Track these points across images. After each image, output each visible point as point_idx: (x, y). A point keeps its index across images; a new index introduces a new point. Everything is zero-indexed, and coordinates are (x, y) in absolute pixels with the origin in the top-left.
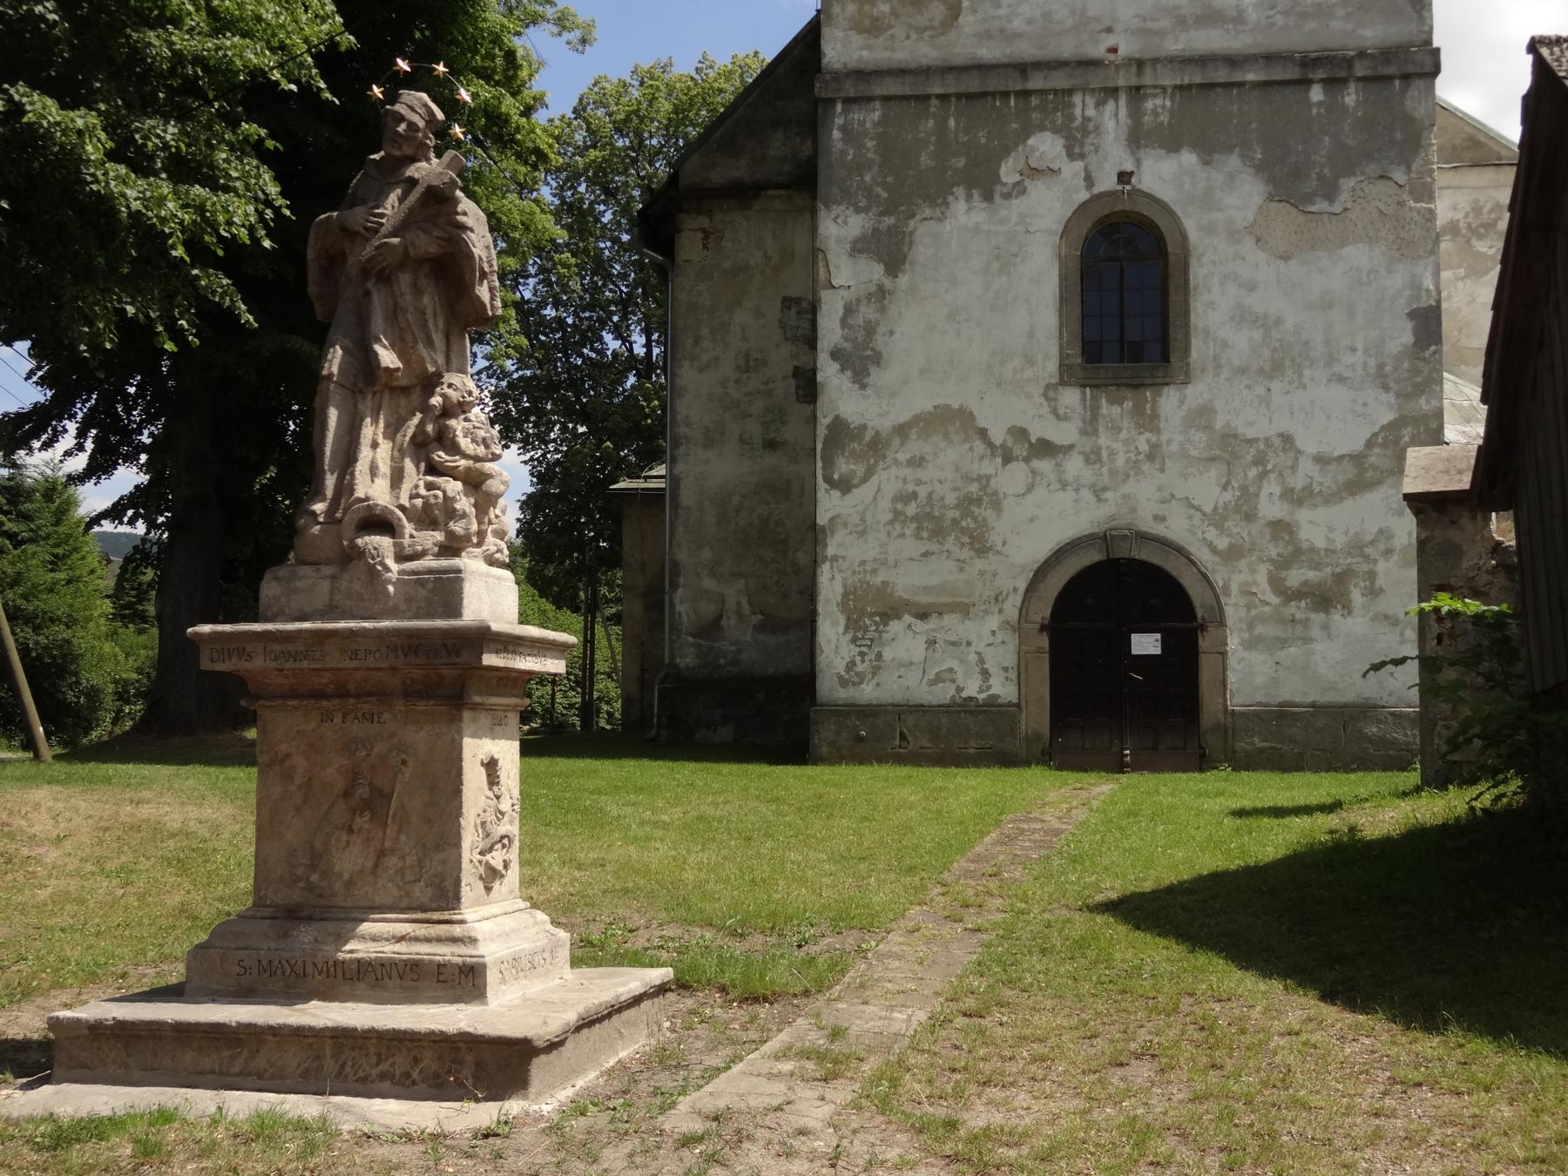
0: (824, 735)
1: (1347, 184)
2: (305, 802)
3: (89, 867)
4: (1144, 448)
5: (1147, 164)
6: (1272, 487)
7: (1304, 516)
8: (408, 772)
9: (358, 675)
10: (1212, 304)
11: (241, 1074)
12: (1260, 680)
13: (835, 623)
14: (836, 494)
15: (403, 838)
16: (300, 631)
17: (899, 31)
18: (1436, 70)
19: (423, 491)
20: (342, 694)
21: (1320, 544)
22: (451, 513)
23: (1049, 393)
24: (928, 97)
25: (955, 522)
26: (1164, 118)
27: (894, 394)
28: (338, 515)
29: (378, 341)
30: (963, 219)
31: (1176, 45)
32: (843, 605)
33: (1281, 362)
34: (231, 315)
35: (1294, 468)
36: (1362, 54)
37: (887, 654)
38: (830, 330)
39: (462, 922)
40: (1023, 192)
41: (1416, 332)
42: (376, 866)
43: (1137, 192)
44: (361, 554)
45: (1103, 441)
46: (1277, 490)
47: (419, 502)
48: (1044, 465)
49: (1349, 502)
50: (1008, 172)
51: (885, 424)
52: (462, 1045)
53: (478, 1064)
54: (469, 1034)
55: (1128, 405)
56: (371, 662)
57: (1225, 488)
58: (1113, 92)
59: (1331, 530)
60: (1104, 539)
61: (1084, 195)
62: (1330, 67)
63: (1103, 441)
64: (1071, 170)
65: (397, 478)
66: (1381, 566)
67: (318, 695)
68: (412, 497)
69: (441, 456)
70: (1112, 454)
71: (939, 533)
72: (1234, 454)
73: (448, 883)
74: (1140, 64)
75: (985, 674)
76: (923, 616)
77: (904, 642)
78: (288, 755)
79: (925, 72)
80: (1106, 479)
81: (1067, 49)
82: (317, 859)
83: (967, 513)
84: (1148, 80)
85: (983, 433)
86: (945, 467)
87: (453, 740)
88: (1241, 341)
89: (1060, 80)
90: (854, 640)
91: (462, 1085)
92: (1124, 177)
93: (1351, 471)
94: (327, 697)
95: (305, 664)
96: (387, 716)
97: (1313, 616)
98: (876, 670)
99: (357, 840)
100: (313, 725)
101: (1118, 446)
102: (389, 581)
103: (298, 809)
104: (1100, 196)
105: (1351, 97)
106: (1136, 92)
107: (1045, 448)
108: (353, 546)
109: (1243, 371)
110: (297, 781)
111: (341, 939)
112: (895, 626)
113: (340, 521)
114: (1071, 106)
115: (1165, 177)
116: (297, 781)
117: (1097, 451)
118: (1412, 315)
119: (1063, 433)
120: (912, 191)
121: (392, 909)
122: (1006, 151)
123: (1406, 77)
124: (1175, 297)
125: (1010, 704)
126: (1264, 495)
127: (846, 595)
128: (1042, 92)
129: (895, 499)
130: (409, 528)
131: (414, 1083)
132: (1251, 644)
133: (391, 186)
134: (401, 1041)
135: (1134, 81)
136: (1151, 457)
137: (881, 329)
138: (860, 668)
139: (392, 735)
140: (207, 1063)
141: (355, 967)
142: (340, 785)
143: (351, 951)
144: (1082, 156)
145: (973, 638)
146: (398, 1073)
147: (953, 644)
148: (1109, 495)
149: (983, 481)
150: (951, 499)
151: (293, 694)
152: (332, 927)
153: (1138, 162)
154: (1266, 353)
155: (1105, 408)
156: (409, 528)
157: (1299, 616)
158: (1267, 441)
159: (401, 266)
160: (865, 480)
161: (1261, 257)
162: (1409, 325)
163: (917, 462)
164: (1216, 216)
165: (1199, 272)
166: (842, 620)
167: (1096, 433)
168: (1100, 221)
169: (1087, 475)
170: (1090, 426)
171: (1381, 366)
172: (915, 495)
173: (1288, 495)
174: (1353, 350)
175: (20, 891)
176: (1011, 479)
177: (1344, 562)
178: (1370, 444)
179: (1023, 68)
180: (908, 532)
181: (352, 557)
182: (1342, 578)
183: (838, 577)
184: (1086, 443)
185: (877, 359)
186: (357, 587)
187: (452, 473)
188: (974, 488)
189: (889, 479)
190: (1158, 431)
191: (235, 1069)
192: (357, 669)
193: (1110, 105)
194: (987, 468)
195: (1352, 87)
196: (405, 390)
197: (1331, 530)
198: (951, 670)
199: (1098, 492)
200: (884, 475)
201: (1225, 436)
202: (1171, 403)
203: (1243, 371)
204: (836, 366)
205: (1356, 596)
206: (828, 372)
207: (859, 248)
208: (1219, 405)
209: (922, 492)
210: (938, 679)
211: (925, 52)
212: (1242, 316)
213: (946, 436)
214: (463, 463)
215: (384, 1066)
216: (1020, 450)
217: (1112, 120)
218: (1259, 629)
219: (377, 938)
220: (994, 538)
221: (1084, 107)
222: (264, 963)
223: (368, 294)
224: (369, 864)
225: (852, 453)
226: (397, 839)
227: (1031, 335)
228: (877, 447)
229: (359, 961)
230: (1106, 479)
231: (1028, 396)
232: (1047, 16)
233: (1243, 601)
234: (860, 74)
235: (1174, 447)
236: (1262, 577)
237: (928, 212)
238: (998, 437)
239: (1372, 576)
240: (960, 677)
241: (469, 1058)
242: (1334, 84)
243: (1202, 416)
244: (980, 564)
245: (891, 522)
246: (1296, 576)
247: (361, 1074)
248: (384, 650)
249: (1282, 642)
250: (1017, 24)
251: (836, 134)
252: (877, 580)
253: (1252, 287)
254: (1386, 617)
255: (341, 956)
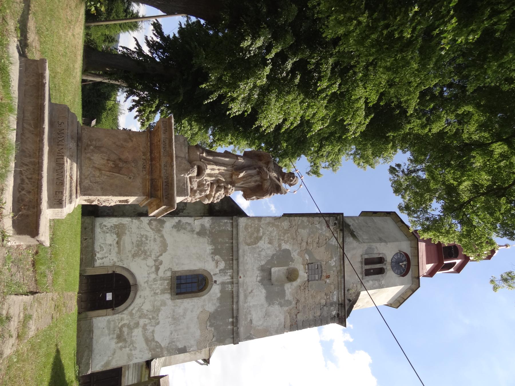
0: (88, 220)
1: (213, 329)
2: (117, 145)
3: (67, 44)
4: (157, 291)
5: (218, 286)
6: (147, 321)
7: (140, 329)
8: (127, 179)
9: (158, 165)
10: (188, 303)
11: (23, 127)
12: (99, 324)
13: (116, 222)
14: (148, 222)
15: (105, 177)
16: (173, 150)
17: (245, 233)
18: (234, 344)
19: (207, 183)
20: (152, 159)
21: (133, 334)
22: (201, 191)
23: (170, 269)
24: (232, 240)
25: (141, 249)
26: (227, 289)
27: (170, 234)
28: (202, 160)
29: (246, 172)
30: (208, 248)
31: (241, 290)
32: (121, 224)
33: (175, 319)
34: (208, 98)
35: (152, 326)
36: (238, 328)
37: (108, 235)
38: (185, 220)
39: (77, 197)
40: (213, 261)
41: (181, 348)
42: (96, 168)
43: (212, 284)
44: (192, 167)
45: (159, 282)
46: (146, 323)
47: (205, 182)
48: (153, 269)
49: (143, 339)
50: (217, 257)
51: (164, 233)
52: (35, 210)
53: (28, 216)
54: (40, 213)
55: (167, 287)
56: (163, 171)
57: (147, 311)
58: (232, 278)
59: (137, 336)
60: (136, 285)
61: (212, 274)
62: (235, 323)
63: (159, 282)
64: (217, 271)
65: (210, 175)
66: (127, 349)
67: (151, 152)
68: (206, 180)
69: (215, 187)
70: (156, 284)
71: (138, 246)
72: (155, 312)
73: (90, 192)
74: (238, 283)
75: (102, 258)
76: (117, 243)
77: (111, 239)
78: (132, 141)
79: (237, 239)
80: (150, 283)
81: (241, 268)
82: (98, 148)
83: (142, 252)
84: (235, 285)
85: (161, 255)
86: (154, 247)
87: (137, 194)
88: (180, 311)
89: (235, 267)
90: (112, 227)
91: (19, 210)
92: (215, 282)
93: (150, 339)
94: (151, 155)
95: (162, 150)
96: (145, 173)
97: (115, 335)
98: (104, 232)
99: (104, 162)
100: (142, 149)
101: (157, 286)
102: (185, 175)
103: (115, 143)
104: (212, 277)
105: (230, 327)
106: (232, 283)
107: (157, 269)
108: (195, 165)
109: (174, 312)
110: (124, 143)
111: (71, 157)
112: (115, 236)
113: (201, 161)
114: (230, 269)
115: (215, 290)
116: (124, 143)
117: (156, 281)
118: (185, 347)
119: (161, 273)
120: (213, 236)
121: (81, 173)
122: (221, 256)
123: (233, 338)
124: (190, 295)
125: (94, 265)
126: (145, 320)
127: (123, 224)
128: (233, 264)
129: (146, 236)
130: (198, 180)
131: (20, 192)
132: (109, 322)
133: (278, 174)
134: (37, 187)
135: (234, 282)
136: (155, 293)
137: (185, 231)
138: (104, 228)
139: (139, 174)
140: (28, 115)
141: (61, 162)
142: (123, 157)
143: (67, 161)
144: (220, 273)
145: (112, 255)
146: (24, 186)
147: (110, 250)
148: (146, 284)
149: (150, 256)
150: (146, 248)
151: (151, 144)
152: (75, 154)
153: (218, 284)
154: (178, 316)
155: (166, 282)
156: (198, 180)
157: (115, 332)
158: (158, 319)
159: (261, 178)
160: (151, 228)
161: (198, 312)
162: (183, 347)
163: (155, 240)
164: (207, 302)
165: (195, 299)
166: (116, 224)
167: (161, 280)
168: (206, 277)
169: (151, 279)
170: (162, 279)
171: (174, 342)
172: (147, 240)
173: (145, 325)
174: (178, 335)
175: (62, 26)
176: (150, 262)
177: (129, 340)
178: (157, 342)
179: (237, 259)
180: (138, 239)
181: (191, 163)
182: (125, 340)
183: (127, 222)
184: (158, 278)
185: (178, 230)
186: (183, 165)
187: (211, 191)
188: (148, 253)
189: (151, 234)
190: (161, 294)
191: (25, 125)
192: (160, 165)
193: (230, 278)
194: (153, 256)
195: (232, 327)
196: (231, 177)
197: (137, 336)
198: (103, 250)
199: (147, 282)
200: (152, 233)
201: (159, 309)
202: (167, 296)
203: (174, 312)
204: (177, 221)
205: (120, 344)
206: (176, 219)
207: (202, 226)
208: (166, 307)
209: (148, 242)
210: (101, 247)
211: (241, 239)
212: (185, 310)
213: (161, 246)
214: (213, 194)
215: (27, 181)
216: (157, 263)
217: (227, 278)
218: (112, 323)
219: (71, 169)
220: (136, 259)
221: (230, 272)
222: (63, 131)
223: (255, 169)
224: (96, 166)
225: (157, 225)
226: (105, 175)
227: (183, 264)
228: (159, 231)
229: (64, 164)
230: (150, 283)
231: (169, 264)
232: (247, 263)
233: (120, 318)
234: (237, 225)
235: (157, 298)
236: (125, 322)
237: (209, 240)
238: (160, 258)
239: (125, 347)
240: (102, 252)
241: (30, 213)
242: (233, 323)
243: (164, 304)
244: (130, 256)
245: (141, 235)
246: (125, 330)
247: (23, 172)
248: (167, 175)
249: (109, 329)
250: (246, 257)
251: (226, 221)
252: (127, 232)
253: (192, 311)
254: (115, 352)
255: (65, 158)
